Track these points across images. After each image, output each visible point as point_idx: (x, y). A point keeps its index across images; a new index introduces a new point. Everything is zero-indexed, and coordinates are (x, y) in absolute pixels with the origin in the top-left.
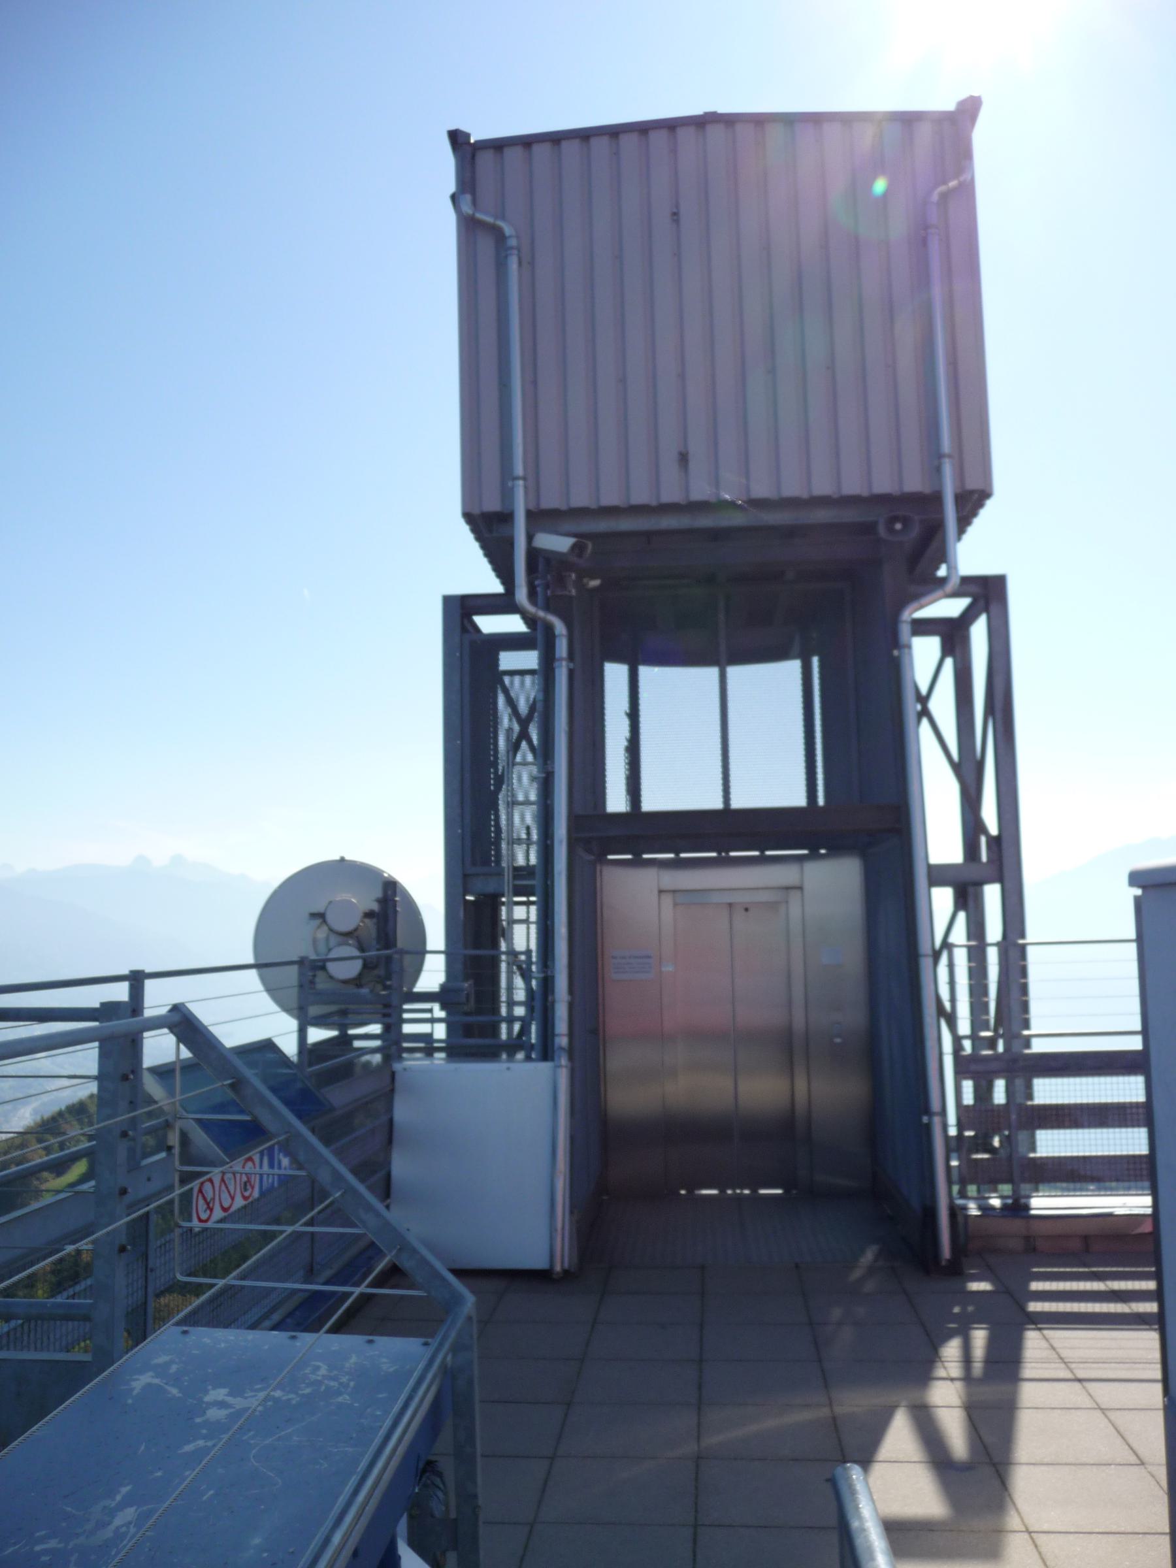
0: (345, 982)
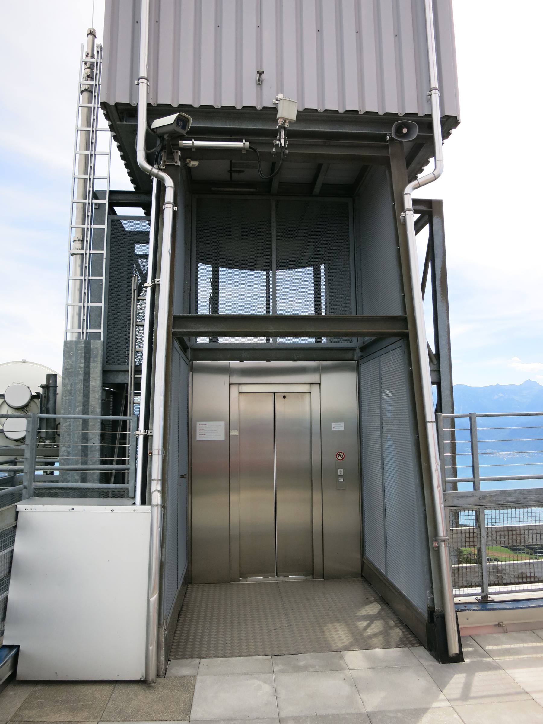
0: (17, 440)
